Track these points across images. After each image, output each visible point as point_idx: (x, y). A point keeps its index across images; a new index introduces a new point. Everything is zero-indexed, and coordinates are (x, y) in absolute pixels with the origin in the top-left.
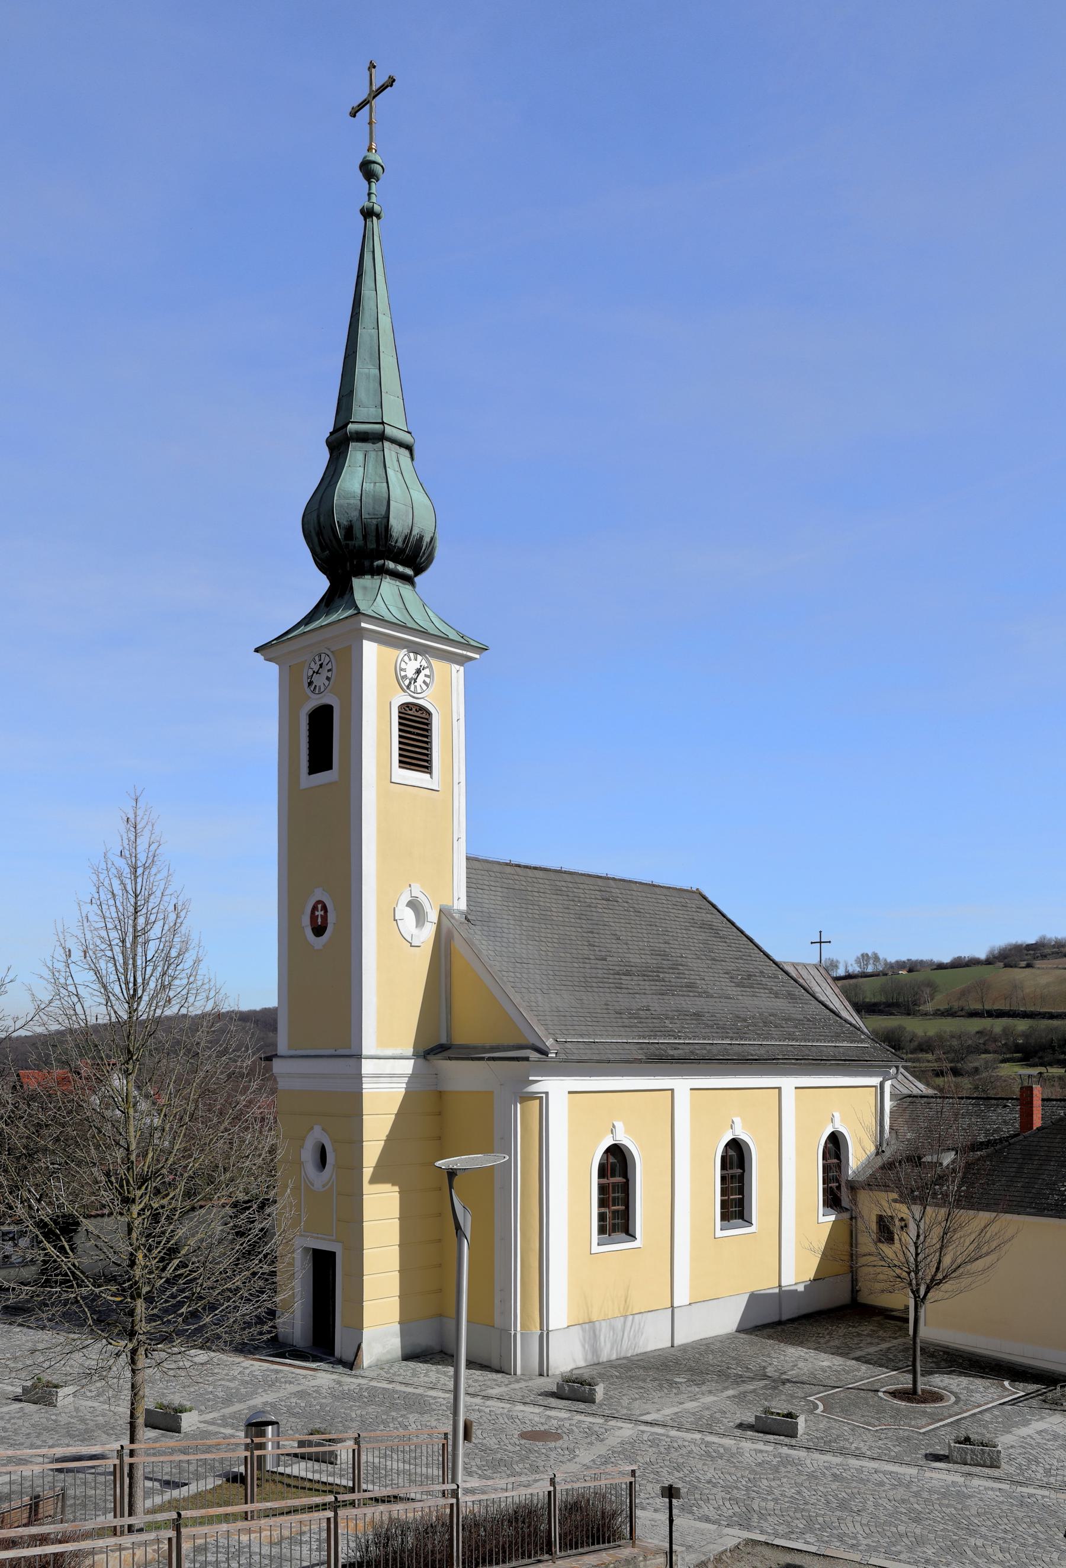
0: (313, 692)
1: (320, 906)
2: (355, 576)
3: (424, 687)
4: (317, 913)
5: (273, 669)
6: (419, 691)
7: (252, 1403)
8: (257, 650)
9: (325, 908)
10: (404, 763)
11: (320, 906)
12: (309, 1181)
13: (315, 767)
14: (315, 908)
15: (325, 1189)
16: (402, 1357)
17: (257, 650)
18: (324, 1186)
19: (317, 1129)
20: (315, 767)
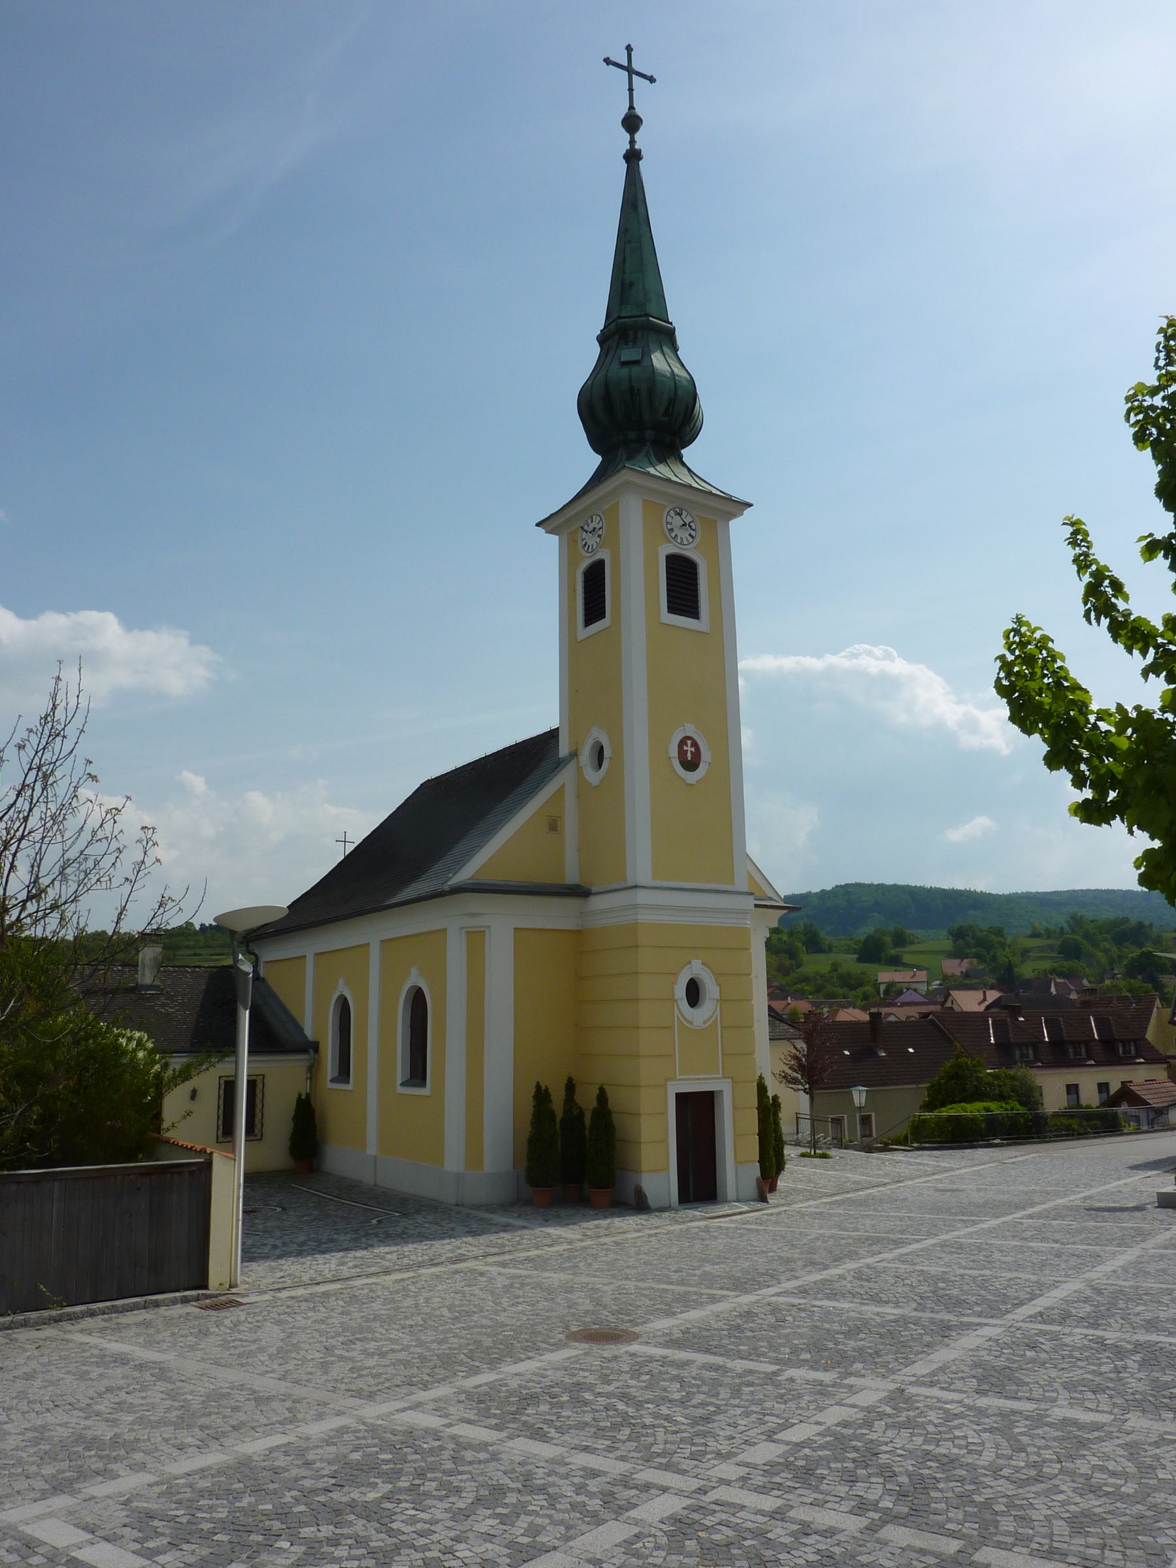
0: (587, 552)
1: (689, 742)
2: (683, 448)
3: (691, 540)
4: (685, 748)
5: (555, 539)
6: (686, 543)
7: (1097, 1274)
8: (538, 525)
9: (695, 744)
10: (672, 609)
11: (689, 742)
12: (685, 1019)
13: (589, 620)
14: (683, 742)
15: (706, 1025)
16: (1158, 1202)
17: (538, 525)
18: (705, 1022)
19: (414, 971)
20: (589, 620)
